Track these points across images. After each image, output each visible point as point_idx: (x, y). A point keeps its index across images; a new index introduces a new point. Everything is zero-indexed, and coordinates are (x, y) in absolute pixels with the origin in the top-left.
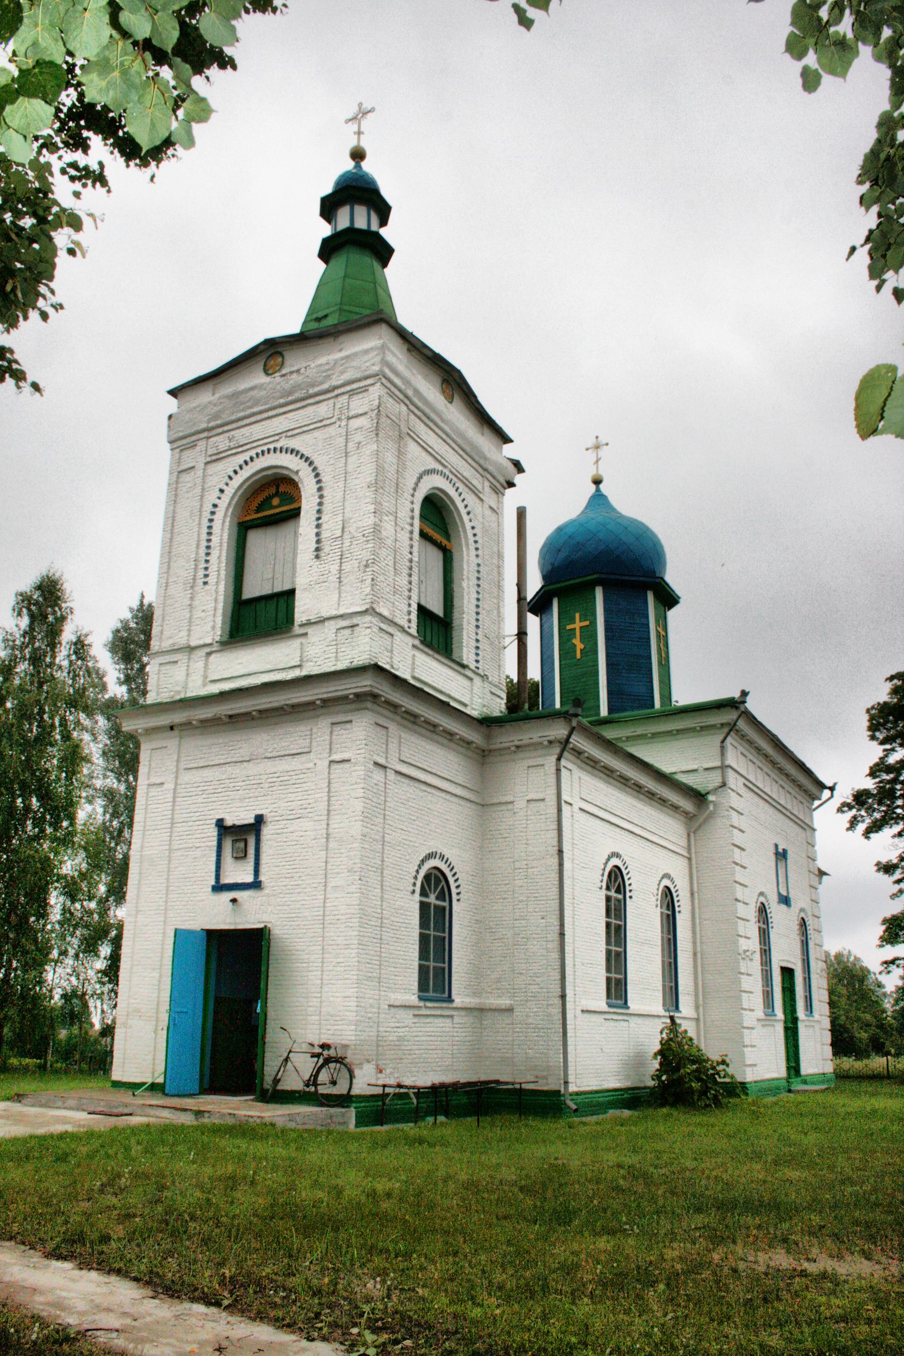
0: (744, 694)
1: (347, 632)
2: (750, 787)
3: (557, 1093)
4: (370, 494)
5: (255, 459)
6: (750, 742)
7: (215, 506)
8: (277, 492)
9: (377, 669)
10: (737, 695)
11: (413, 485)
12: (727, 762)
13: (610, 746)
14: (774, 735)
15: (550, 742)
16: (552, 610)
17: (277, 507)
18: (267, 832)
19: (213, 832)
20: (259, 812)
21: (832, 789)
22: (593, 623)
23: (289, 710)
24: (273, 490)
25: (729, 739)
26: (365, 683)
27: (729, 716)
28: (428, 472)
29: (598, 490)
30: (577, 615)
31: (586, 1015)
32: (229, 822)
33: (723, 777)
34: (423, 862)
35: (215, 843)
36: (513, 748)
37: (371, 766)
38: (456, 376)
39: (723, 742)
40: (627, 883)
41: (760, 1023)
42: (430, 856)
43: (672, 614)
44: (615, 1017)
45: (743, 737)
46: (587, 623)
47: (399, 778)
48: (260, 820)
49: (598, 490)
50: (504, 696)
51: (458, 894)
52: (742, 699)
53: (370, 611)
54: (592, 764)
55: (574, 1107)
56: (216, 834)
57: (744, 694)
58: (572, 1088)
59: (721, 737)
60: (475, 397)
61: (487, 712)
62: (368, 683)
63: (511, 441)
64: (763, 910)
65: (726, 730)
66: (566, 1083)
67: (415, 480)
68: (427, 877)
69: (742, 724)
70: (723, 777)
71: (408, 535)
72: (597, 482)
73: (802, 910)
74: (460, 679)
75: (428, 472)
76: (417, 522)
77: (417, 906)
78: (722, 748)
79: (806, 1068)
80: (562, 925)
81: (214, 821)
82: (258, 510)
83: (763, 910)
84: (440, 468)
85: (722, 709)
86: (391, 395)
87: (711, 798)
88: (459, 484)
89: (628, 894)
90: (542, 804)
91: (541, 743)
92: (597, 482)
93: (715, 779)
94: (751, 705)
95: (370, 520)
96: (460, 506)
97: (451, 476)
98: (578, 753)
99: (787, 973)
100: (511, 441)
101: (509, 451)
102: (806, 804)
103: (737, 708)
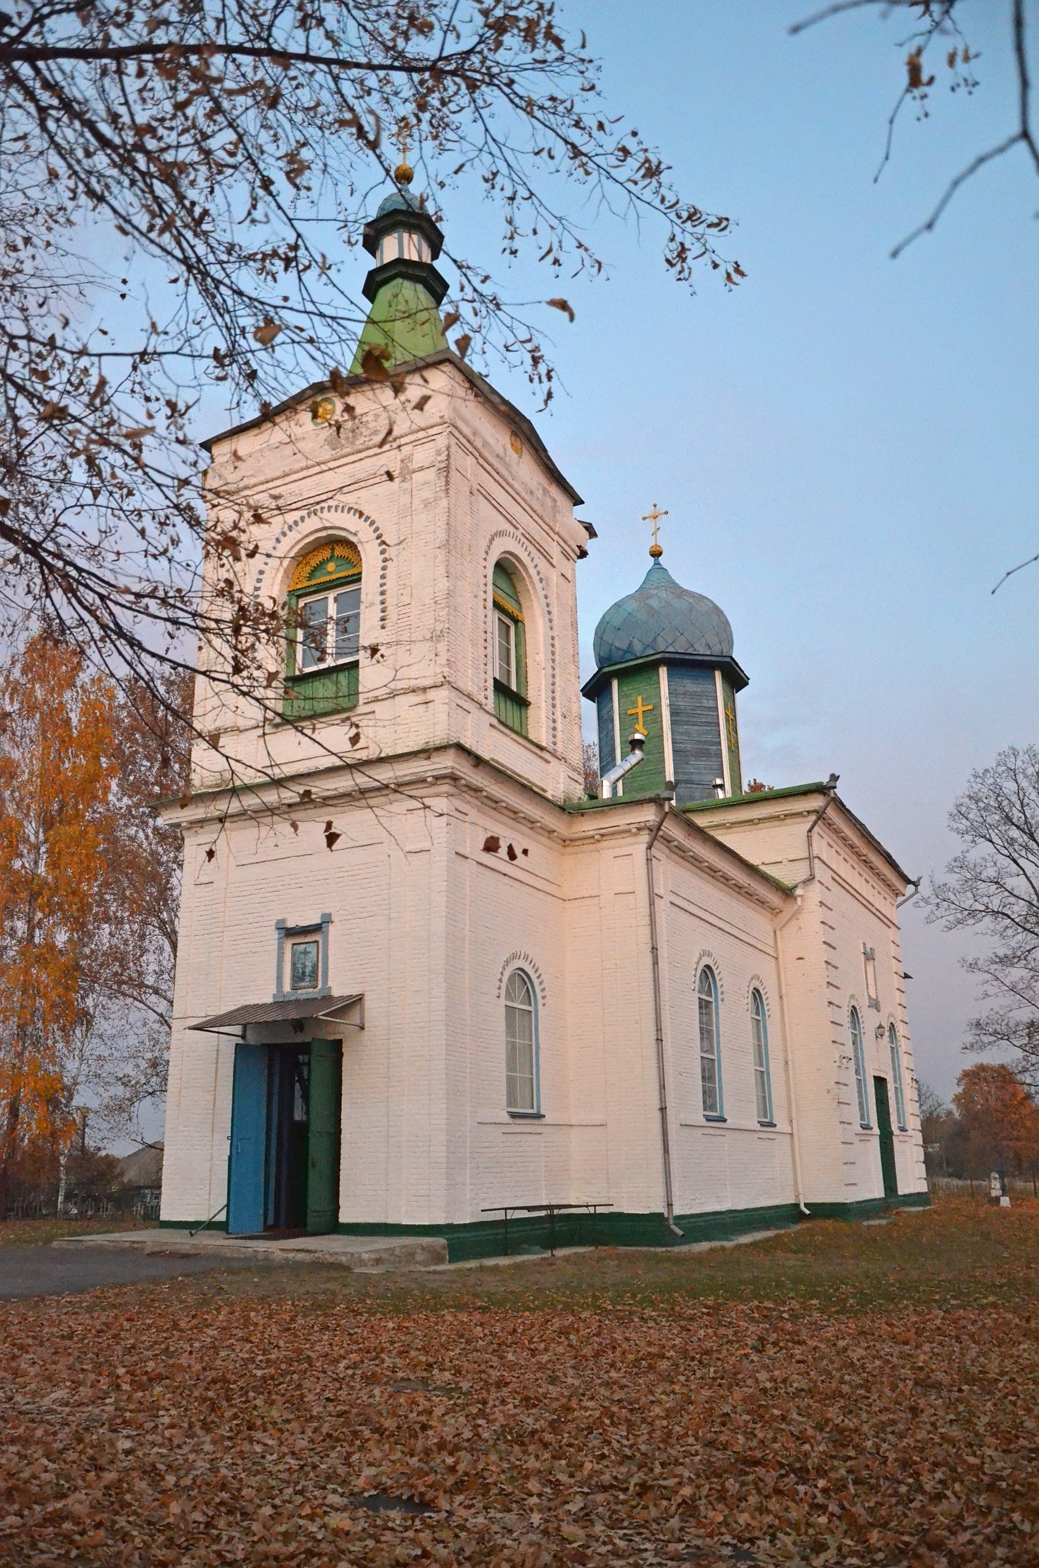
0: (834, 778)
1: (423, 707)
2: (839, 880)
3: (660, 1215)
4: (441, 555)
5: (307, 519)
6: (837, 832)
7: (261, 572)
8: (332, 557)
9: (460, 747)
10: (825, 779)
11: (484, 548)
12: (815, 853)
13: (700, 833)
14: (861, 824)
15: (639, 829)
16: (611, 694)
17: (333, 570)
18: (333, 930)
19: (275, 935)
20: (327, 911)
21: (916, 884)
22: (657, 707)
23: (358, 795)
24: (326, 554)
25: (816, 828)
26: (447, 762)
27: (816, 802)
28: (500, 534)
29: (657, 563)
30: (639, 699)
31: (686, 1130)
32: (290, 924)
33: (811, 868)
34: (507, 962)
35: (276, 947)
36: (597, 837)
37: (454, 856)
38: (525, 426)
39: (810, 831)
40: (719, 984)
41: (858, 1138)
42: (515, 956)
43: (740, 696)
44: (712, 1131)
45: (830, 825)
46: (650, 707)
47: (481, 869)
48: (327, 920)
49: (657, 563)
50: (581, 780)
51: (544, 997)
52: (832, 784)
53: (445, 682)
54: (680, 852)
55: (680, 1233)
56: (276, 936)
57: (834, 778)
58: (677, 1211)
59: (808, 826)
60: (545, 450)
61: (568, 799)
62: (450, 764)
63: (582, 502)
64: (854, 1012)
65: (813, 818)
66: (670, 1205)
67: (487, 541)
68: (511, 979)
69: (831, 813)
70: (811, 868)
71: (482, 603)
72: (656, 554)
73: (890, 1015)
74: (538, 761)
75: (500, 534)
76: (490, 588)
77: (503, 1011)
78: (809, 838)
79: (903, 1189)
80: (659, 1030)
81: (274, 922)
82: (309, 579)
83: (854, 1012)
84: (512, 529)
85: (810, 796)
86: (460, 445)
87: (799, 892)
88: (531, 548)
89: (720, 997)
90: (631, 896)
91: (629, 831)
92: (656, 554)
93: (801, 872)
94: (841, 791)
95: (443, 584)
96: (533, 572)
97: (523, 539)
98: (668, 841)
99: (880, 1082)
100: (582, 502)
101: (580, 512)
102: (889, 899)
103: (825, 794)
